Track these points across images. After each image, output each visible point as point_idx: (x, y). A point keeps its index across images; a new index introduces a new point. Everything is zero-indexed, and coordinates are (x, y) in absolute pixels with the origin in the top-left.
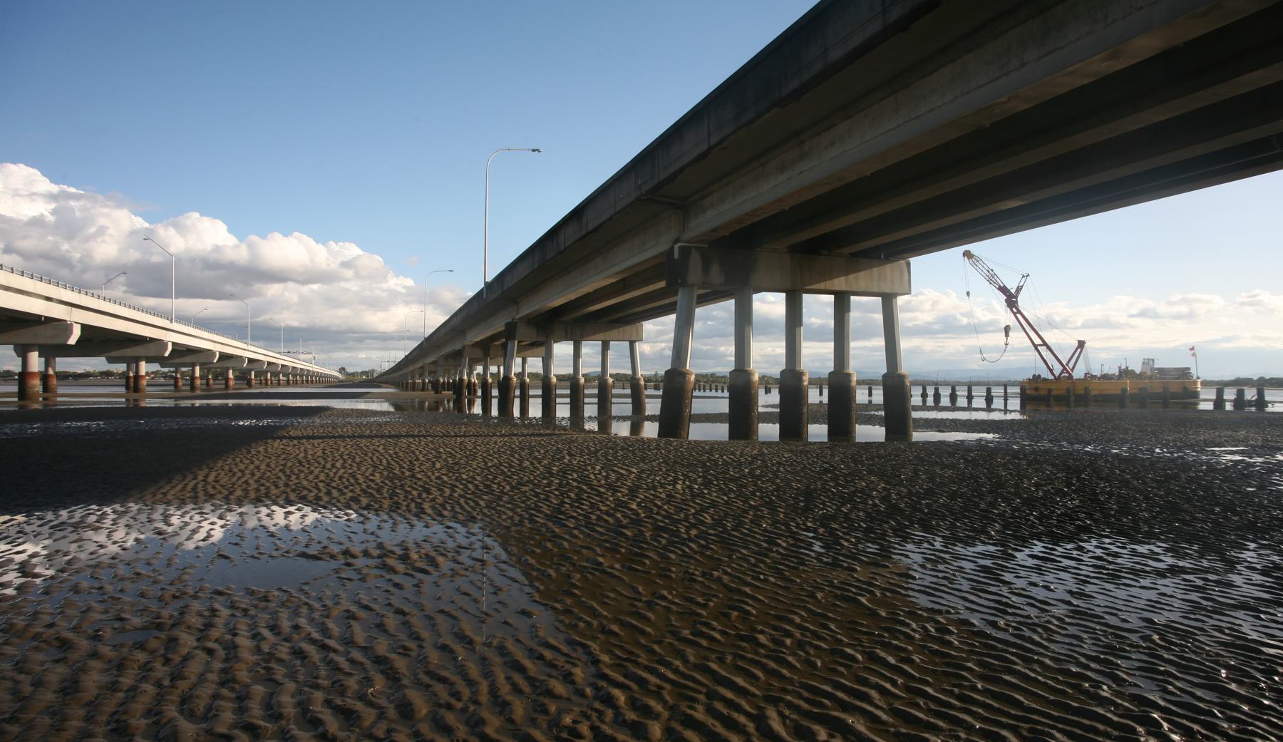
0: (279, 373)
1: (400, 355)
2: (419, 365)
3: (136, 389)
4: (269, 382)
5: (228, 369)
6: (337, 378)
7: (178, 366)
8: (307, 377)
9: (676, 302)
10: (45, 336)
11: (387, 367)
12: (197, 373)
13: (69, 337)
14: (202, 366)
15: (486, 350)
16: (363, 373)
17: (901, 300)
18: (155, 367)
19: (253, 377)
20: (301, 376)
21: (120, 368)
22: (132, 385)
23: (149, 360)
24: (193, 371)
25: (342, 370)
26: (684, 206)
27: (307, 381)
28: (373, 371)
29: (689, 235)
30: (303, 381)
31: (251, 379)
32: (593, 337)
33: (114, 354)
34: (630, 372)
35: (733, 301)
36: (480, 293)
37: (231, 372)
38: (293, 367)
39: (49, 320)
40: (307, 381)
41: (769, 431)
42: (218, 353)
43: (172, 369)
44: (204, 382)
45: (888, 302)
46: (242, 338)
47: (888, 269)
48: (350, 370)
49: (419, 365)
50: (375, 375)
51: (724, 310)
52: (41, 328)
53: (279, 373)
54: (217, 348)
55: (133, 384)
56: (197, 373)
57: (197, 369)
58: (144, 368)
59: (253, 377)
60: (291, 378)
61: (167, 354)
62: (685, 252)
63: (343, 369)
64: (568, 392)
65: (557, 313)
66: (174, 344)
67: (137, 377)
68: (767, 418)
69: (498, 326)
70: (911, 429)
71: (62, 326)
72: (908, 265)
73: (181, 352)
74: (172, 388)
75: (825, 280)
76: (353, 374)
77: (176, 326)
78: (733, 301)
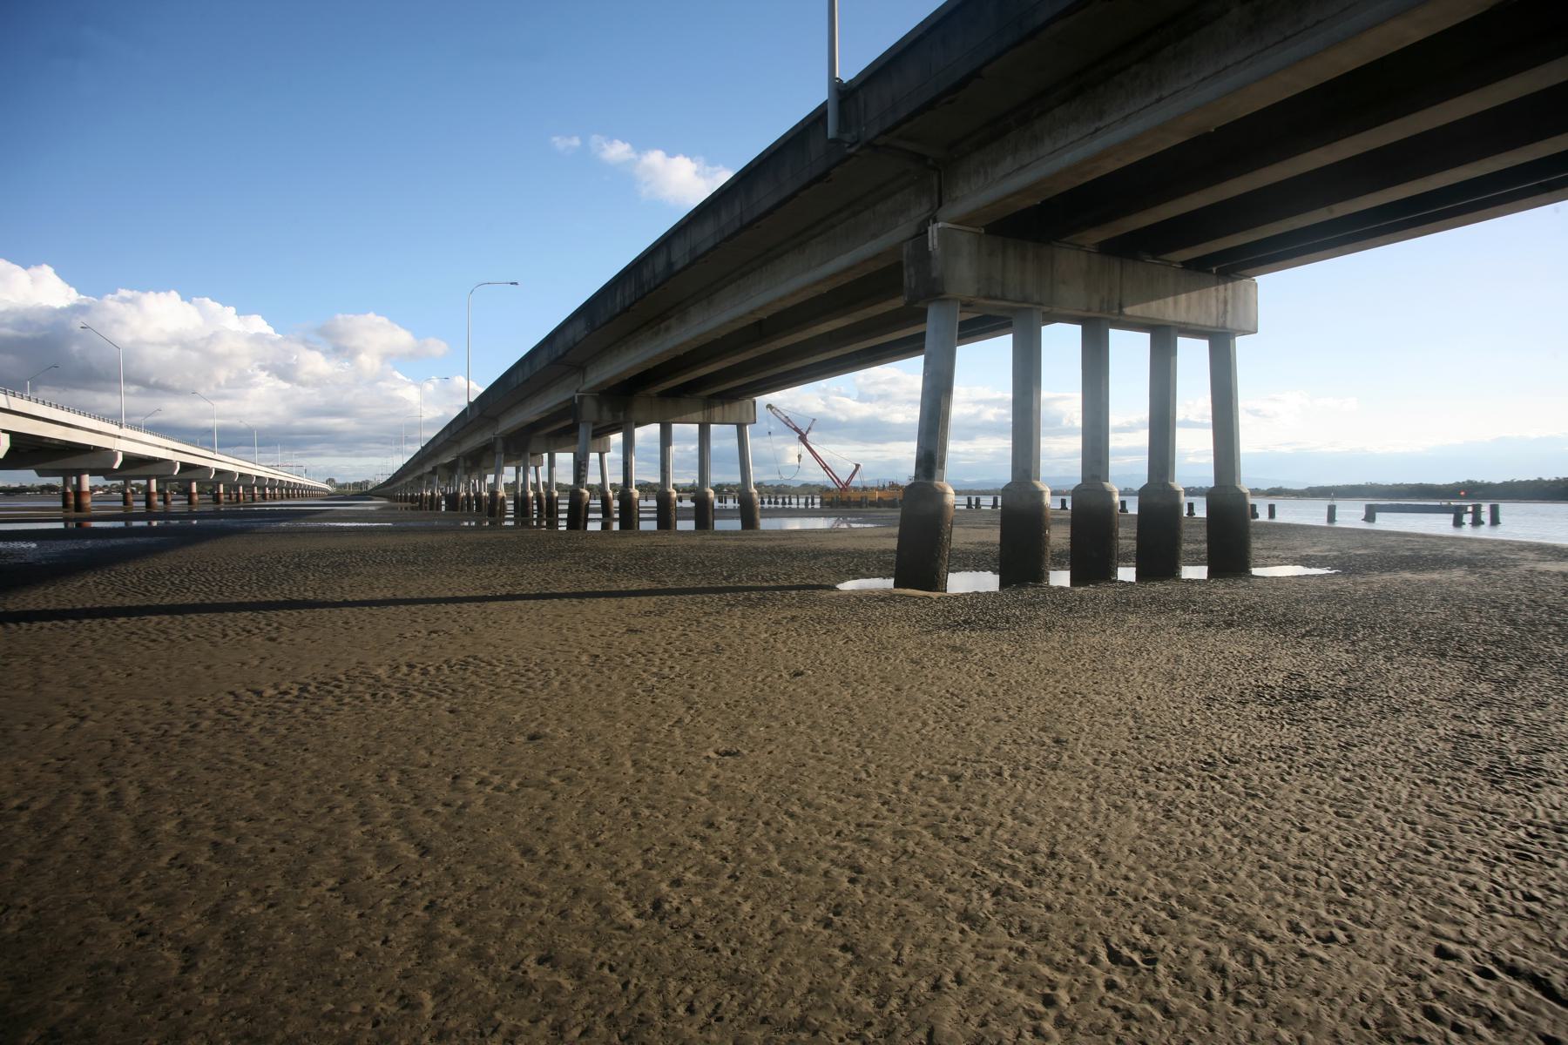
0: (254, 485)
1: (397, 462)
2: (404, 482)
3: (79, 507)
4: (242, 497)
5: (190, 481)
6: (327, 491)
7: (127, 479)
8: (287, 490)
9: (924, 333)
10: (159, 469)
11: (383, 479)
12: (154, 488)
13: (114, 463)
14: (158, 478)
15: (521, 446)
16: (355, 485)
17: (1241, 344)
18: (100, 481)
19: (222, 491)
20: (281, 489)
21: (57, 481)
22: (72, 502)
23: (93, 473)
24: (149, 484)
25: (330, 481)
26: (580, 368)
27: (288, 495)
28: (367, 482)
29: (587, 386)
30: (282, 495)
31: (219, 494)
32: (565, 449)
33: (41, 466)
34: (658, 480)
35: (1011, 336)
36: (464, 413)
37: (194, 484)
38: (270, 479)
39: (162, 460)
40: (288, 495)
41: (649, 525)
42: (178, 464)
43: (119, 482)
44: (161, 497)
45: (1221, 345)
46: (209, 445)
47: (737, 406)
48: (339, 481)
49: (404, 482)
50: (370, 487)
51: (654, 429)
52: (200, 470)
53: (254, 485)
54: (179, 458)
55: (74, 501)
56: (154, 488)
57: (154, 482)
58: (87, 481)
59: (222, 491)
60: (268, 491)
61: (116, 466)
62: (581, 398)
63: (333, 480)
64: (567, 501)
65: (532, 428)
66: (182, 463)
67: (78, 493)
68: (616, 512)
69: (428, 468)
70: (758, 517)
71: (108, 453)
72: (754, 402)
73: (132, 462)
74: (121, 504)
75: (686, 413)
76: (344, 486)
77: (125, 432)
78: (1011, 336)
